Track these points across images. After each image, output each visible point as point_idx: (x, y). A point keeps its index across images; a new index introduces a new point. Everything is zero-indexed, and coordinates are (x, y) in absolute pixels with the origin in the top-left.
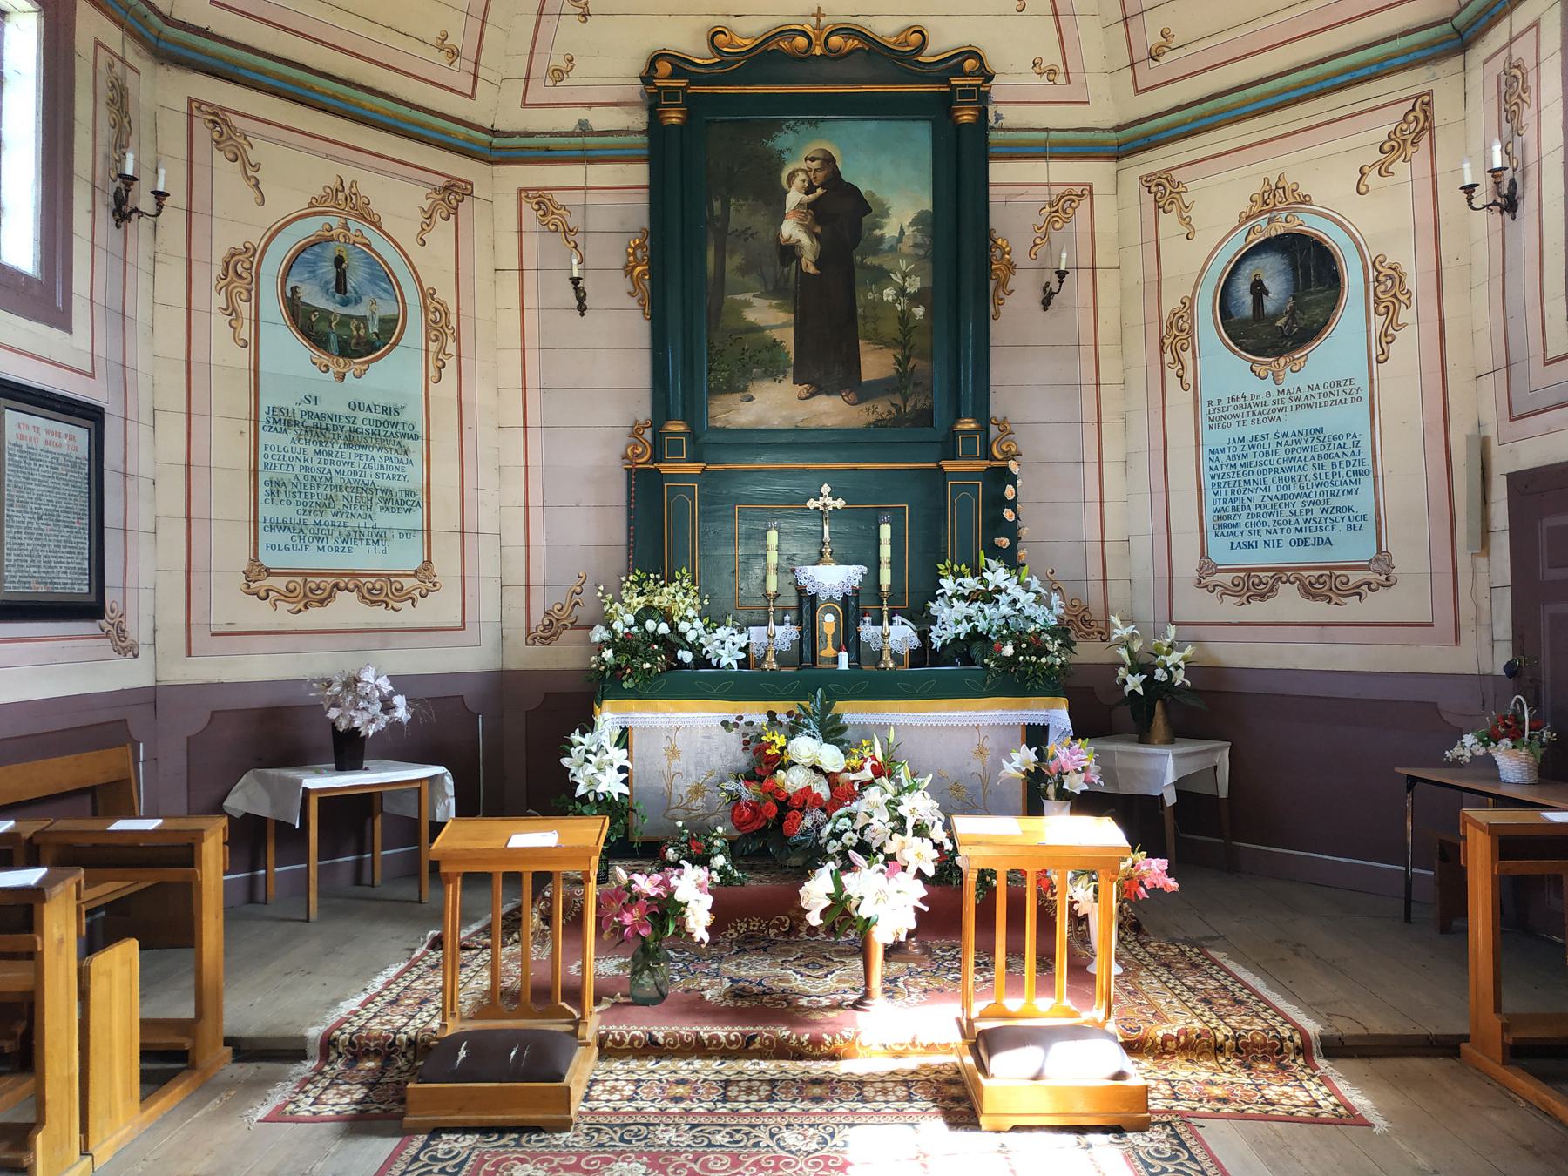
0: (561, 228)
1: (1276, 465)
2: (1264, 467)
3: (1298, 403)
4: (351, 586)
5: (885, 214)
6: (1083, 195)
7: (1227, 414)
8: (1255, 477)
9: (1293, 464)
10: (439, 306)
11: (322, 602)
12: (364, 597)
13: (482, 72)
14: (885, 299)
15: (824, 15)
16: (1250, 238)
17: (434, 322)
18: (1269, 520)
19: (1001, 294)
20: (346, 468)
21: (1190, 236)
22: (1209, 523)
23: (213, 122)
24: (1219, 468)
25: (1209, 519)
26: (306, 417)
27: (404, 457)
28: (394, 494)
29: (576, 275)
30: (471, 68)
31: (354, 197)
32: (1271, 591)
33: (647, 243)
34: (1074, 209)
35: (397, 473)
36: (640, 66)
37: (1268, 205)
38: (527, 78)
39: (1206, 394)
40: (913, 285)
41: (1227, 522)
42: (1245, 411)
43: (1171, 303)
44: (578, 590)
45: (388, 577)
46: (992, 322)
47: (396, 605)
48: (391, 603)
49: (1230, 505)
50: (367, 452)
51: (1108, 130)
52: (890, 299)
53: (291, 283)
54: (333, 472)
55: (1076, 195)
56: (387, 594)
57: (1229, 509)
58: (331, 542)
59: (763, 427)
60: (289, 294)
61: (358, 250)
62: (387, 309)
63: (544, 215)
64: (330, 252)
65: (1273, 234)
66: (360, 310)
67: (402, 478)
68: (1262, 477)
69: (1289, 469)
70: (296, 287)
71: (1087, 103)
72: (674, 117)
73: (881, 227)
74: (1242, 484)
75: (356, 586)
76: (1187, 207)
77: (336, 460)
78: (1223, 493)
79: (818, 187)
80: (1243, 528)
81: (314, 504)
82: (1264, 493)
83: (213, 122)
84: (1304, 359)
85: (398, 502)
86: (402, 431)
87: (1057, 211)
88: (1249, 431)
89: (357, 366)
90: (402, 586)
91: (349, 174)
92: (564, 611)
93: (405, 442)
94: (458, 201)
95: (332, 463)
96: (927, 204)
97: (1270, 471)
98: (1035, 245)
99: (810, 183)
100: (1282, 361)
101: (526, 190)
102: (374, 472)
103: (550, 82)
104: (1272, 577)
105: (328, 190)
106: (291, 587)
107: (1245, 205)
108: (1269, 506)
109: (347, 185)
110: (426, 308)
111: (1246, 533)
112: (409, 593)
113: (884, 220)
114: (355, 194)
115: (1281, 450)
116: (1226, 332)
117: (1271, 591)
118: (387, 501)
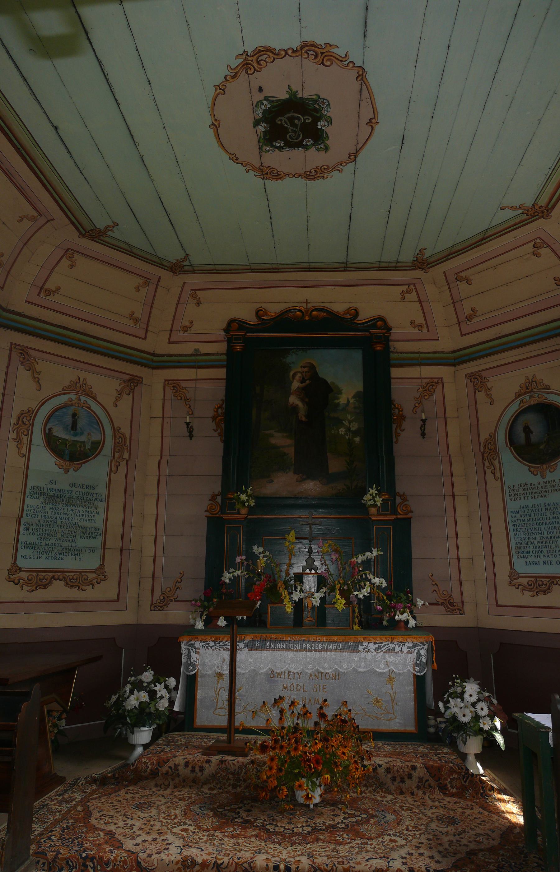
0: (183, 398)
1: (546, 521)
2: (539, 521)
3: (554, 488)
4: (61, 577)
5: (340, 392)
6: (438, 383)
7: (519, 493)
8: (536, 526)
9: (554, 520)
10: (122, 436)
11: (45, 586)
12: (67, 584)
13: (150, 328)
14: (340, 433)
15: (309, 303)
16: (522, 405)
17: (118, 443)
18: (545, 550)
19: (399, 431)
20: (65, 516)
21: (492, 403)
22: (513, 551)
23: (21, 353)
24: (517, 521)
25: (513, 548)
26: (49, 491)
27: (95, 511)
28: (88, 529)
29: (188, 421)
30: (145, 327)
31: (84, 386)
32: (549, 589)
33: (224, 406)
34: (434, 390)
35: (91, 518)
36: (224, 325)
37: (529, 389)
38: (171, 331)
39: (508, 482)
40: (355, 426)
41: (523, 550)
42: (527, 491)
43: (484, 436)
44: (179, 580)
45: (81, 572)
46: (394, 444)
47: (84, 588)
48: (81, 587)
49: (524, 541)
50: (77, 508)
51: (449, 353)
52: (343, 433)
53: (48, 427)
54: (58, 518)
55: (435, 383)
56: (79, 582)
57: (523, 543)
58: (53, 554)
59: (278, 496)
60: (47, 431)
61: (84, 410)
62: (96, 437)
63: (176, 392)
64: (71, 410)
65: (532, 403)
66: (83, 438)
67: (93, 521)
68: (539, 526)
69: (553, 523)
70: (51, 428)
71: (438, 340)
72: (238, 348)
73: (338, 399)
74: (529, 530)
75: (64, 577)
76: (489, 389)
77: (60, 512)
78: (520, 534)
79: (307, 380)
80: (531, 554)
81: (46, 535)
82: (541, 535)
83: (21, 353)
84: (555, 466)
85: (88, 533)
86: (95, 497)
87: (426, 390)
88: (531, 502)
89: (76, 466)
90: (88, 577)
91: (83, 375)
92: (171, 592)
93: (96, 503)
94: (135, 386)
95: (58, 514)
96: (360, 387)
97: (543, 523)
98: (416, 406)
99: (303, 378)
100: (544, 466)
101: (168, 380)
102: (79, 518)
103: (181, 332)
104: (548, 581)
105: (72, 383)
106: (30, 578)
107: (517, 389)
108: (544, 542)
109: (81, 380)
110: (115, 437)
111: (533, 557)
112: (91, 581)
113: (339, 396)
114: (85, 384)
115: (548, 513)
116: (515, 451)
117: (549, 589)
118: (84, 533)
